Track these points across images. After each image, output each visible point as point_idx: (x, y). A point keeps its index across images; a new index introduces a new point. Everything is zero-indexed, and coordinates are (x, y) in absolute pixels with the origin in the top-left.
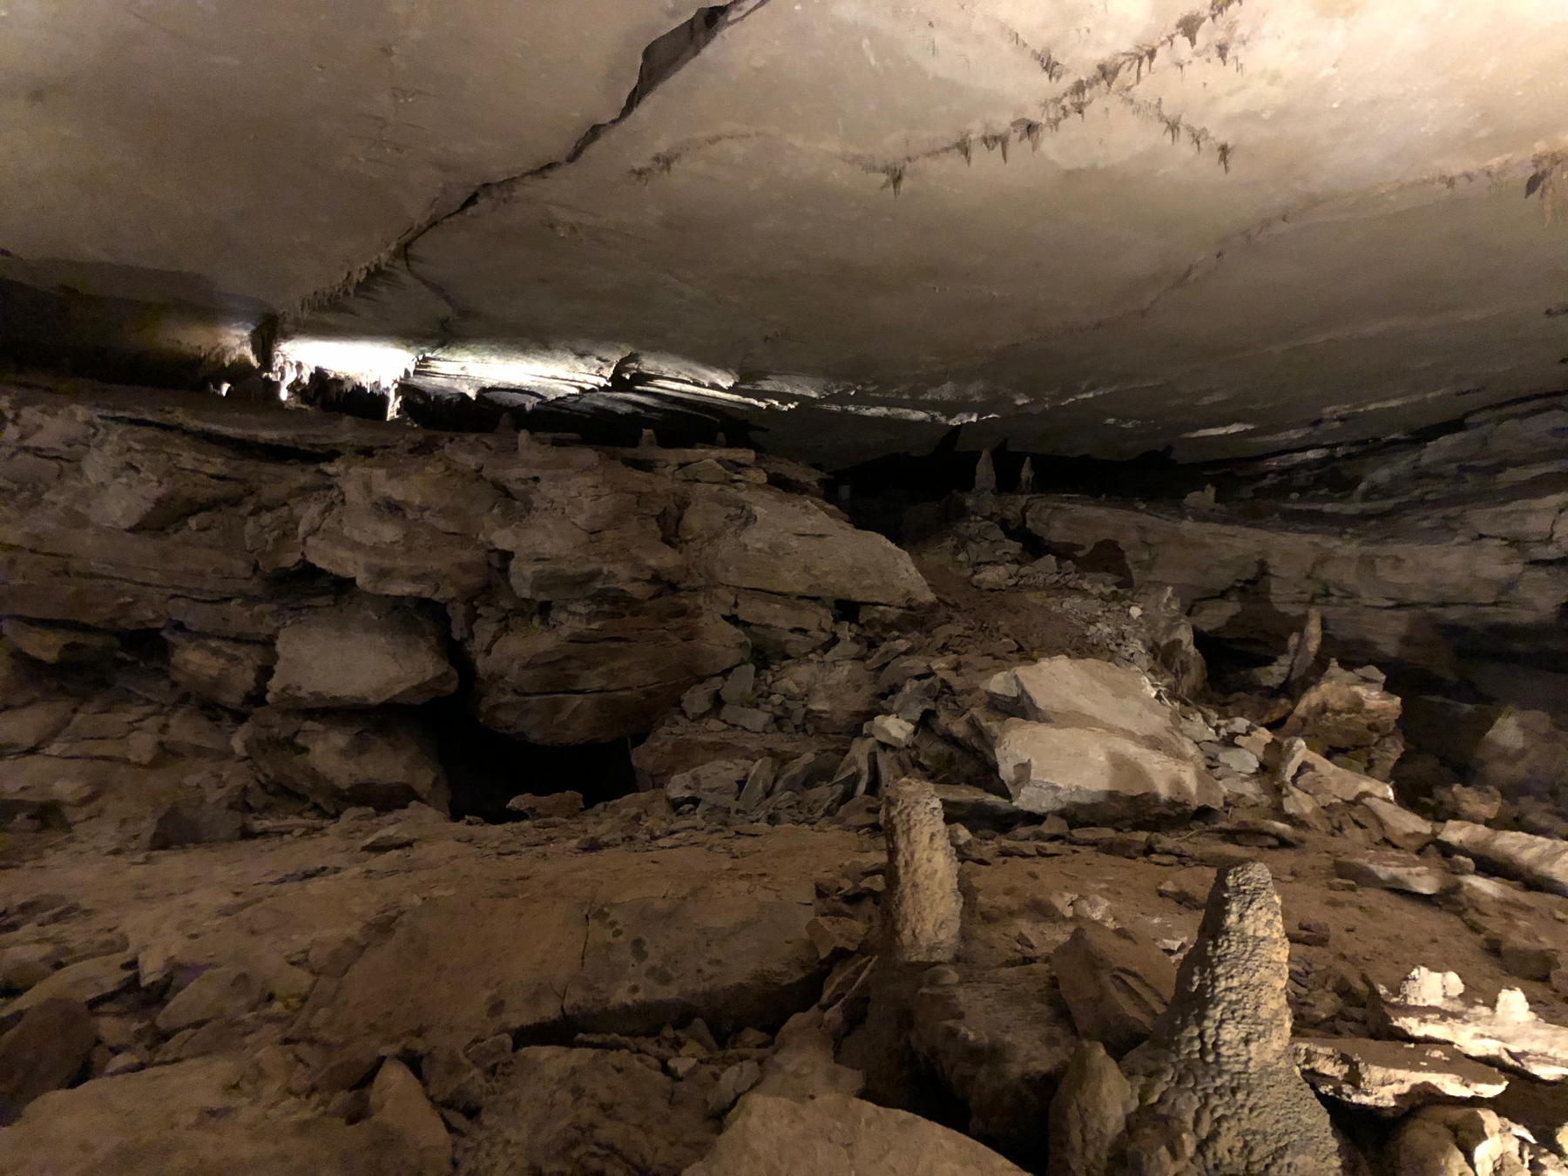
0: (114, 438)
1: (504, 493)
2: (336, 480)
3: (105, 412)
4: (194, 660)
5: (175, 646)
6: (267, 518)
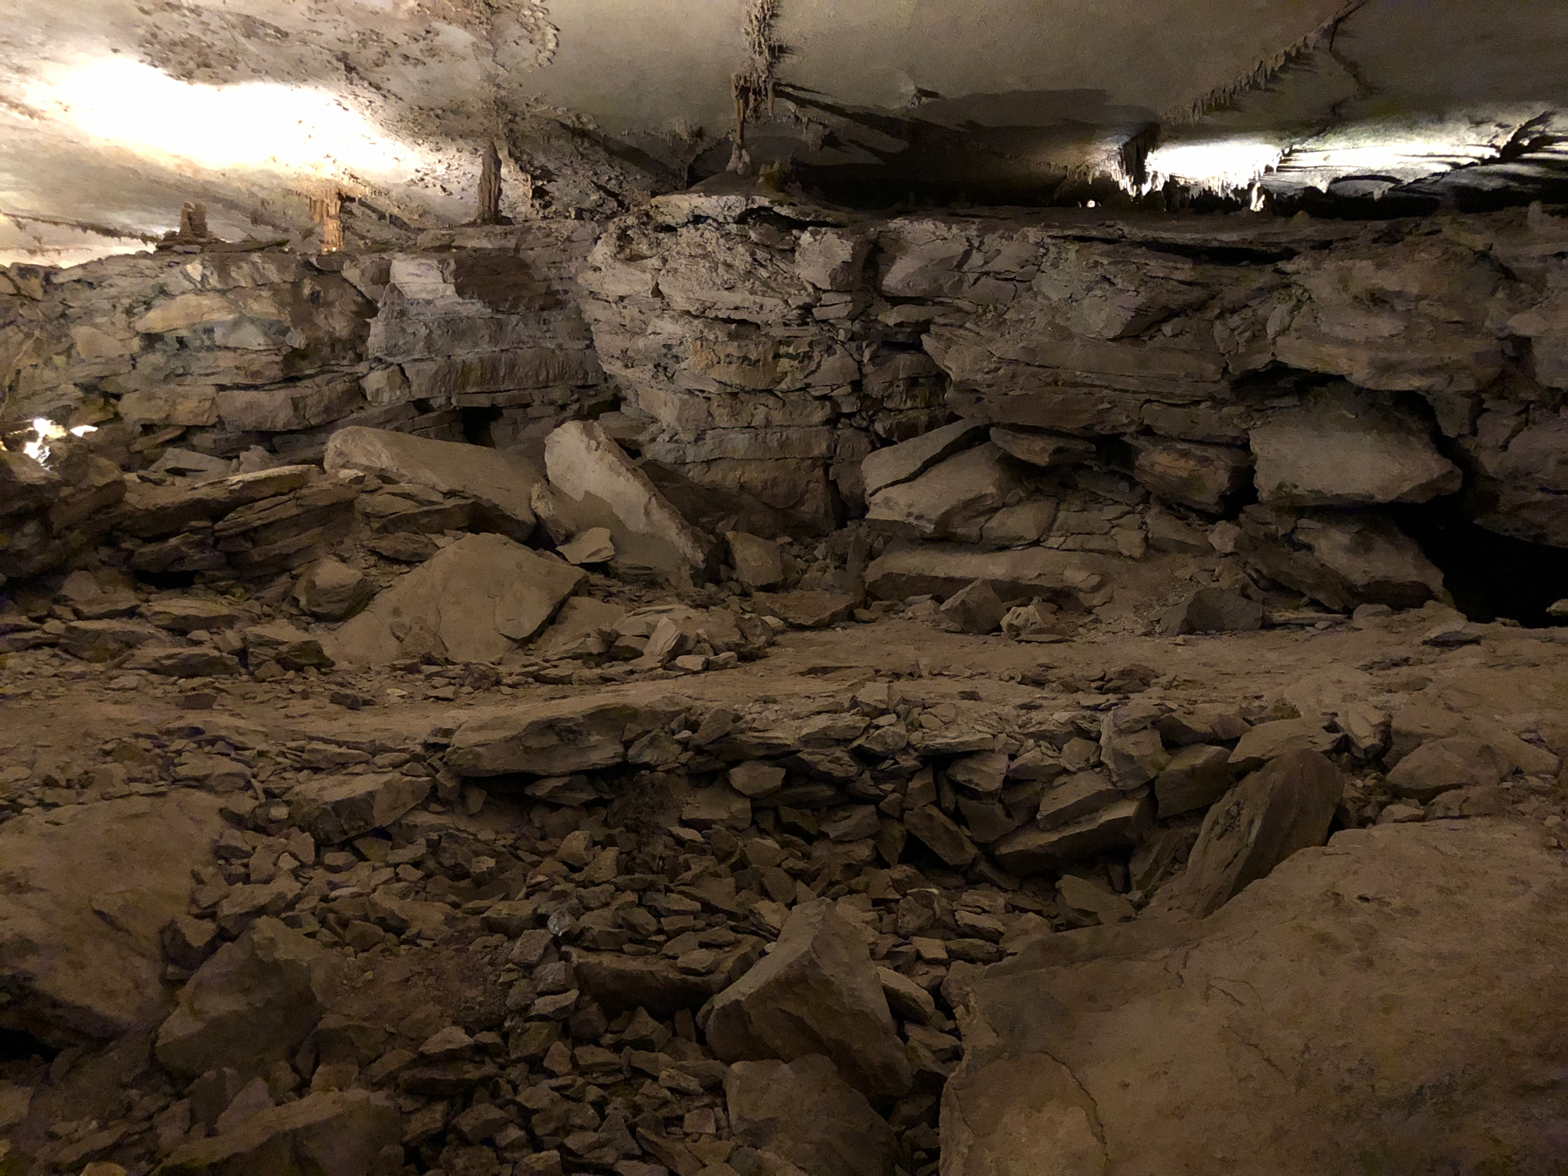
0: (1072, 256)
1: (1507, 274)
2: (1294, 278)
3: (1054, 232)
4: (1161, 462)
5: (1138, 451)
6: (1235, 320)
